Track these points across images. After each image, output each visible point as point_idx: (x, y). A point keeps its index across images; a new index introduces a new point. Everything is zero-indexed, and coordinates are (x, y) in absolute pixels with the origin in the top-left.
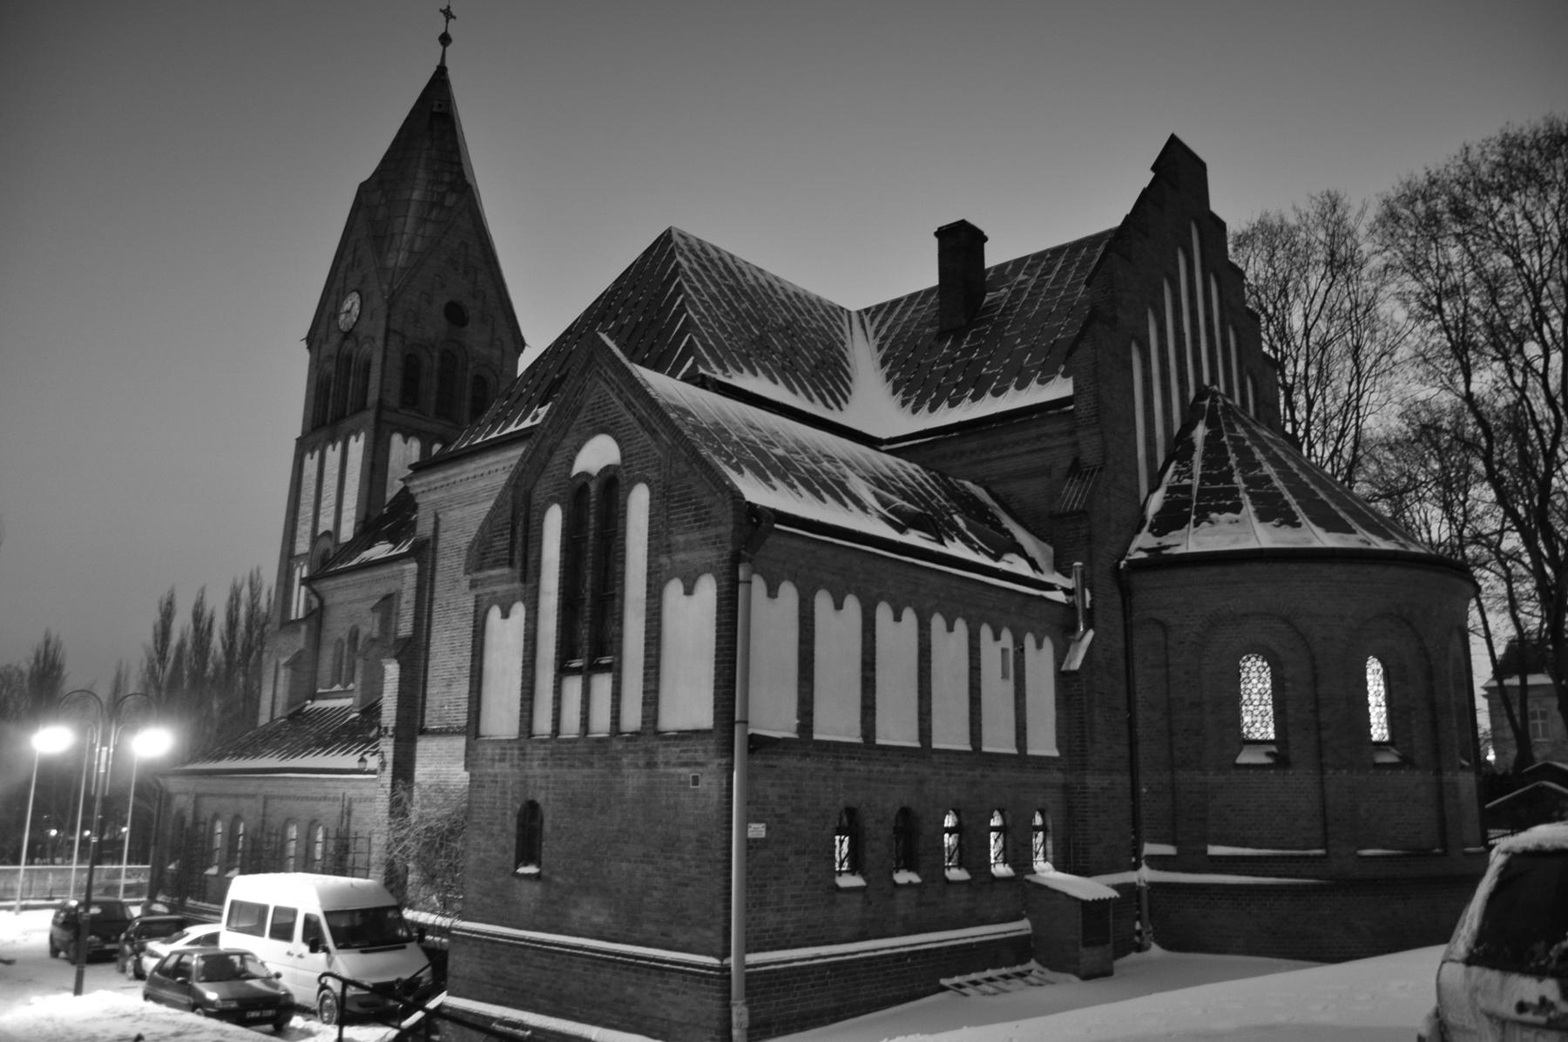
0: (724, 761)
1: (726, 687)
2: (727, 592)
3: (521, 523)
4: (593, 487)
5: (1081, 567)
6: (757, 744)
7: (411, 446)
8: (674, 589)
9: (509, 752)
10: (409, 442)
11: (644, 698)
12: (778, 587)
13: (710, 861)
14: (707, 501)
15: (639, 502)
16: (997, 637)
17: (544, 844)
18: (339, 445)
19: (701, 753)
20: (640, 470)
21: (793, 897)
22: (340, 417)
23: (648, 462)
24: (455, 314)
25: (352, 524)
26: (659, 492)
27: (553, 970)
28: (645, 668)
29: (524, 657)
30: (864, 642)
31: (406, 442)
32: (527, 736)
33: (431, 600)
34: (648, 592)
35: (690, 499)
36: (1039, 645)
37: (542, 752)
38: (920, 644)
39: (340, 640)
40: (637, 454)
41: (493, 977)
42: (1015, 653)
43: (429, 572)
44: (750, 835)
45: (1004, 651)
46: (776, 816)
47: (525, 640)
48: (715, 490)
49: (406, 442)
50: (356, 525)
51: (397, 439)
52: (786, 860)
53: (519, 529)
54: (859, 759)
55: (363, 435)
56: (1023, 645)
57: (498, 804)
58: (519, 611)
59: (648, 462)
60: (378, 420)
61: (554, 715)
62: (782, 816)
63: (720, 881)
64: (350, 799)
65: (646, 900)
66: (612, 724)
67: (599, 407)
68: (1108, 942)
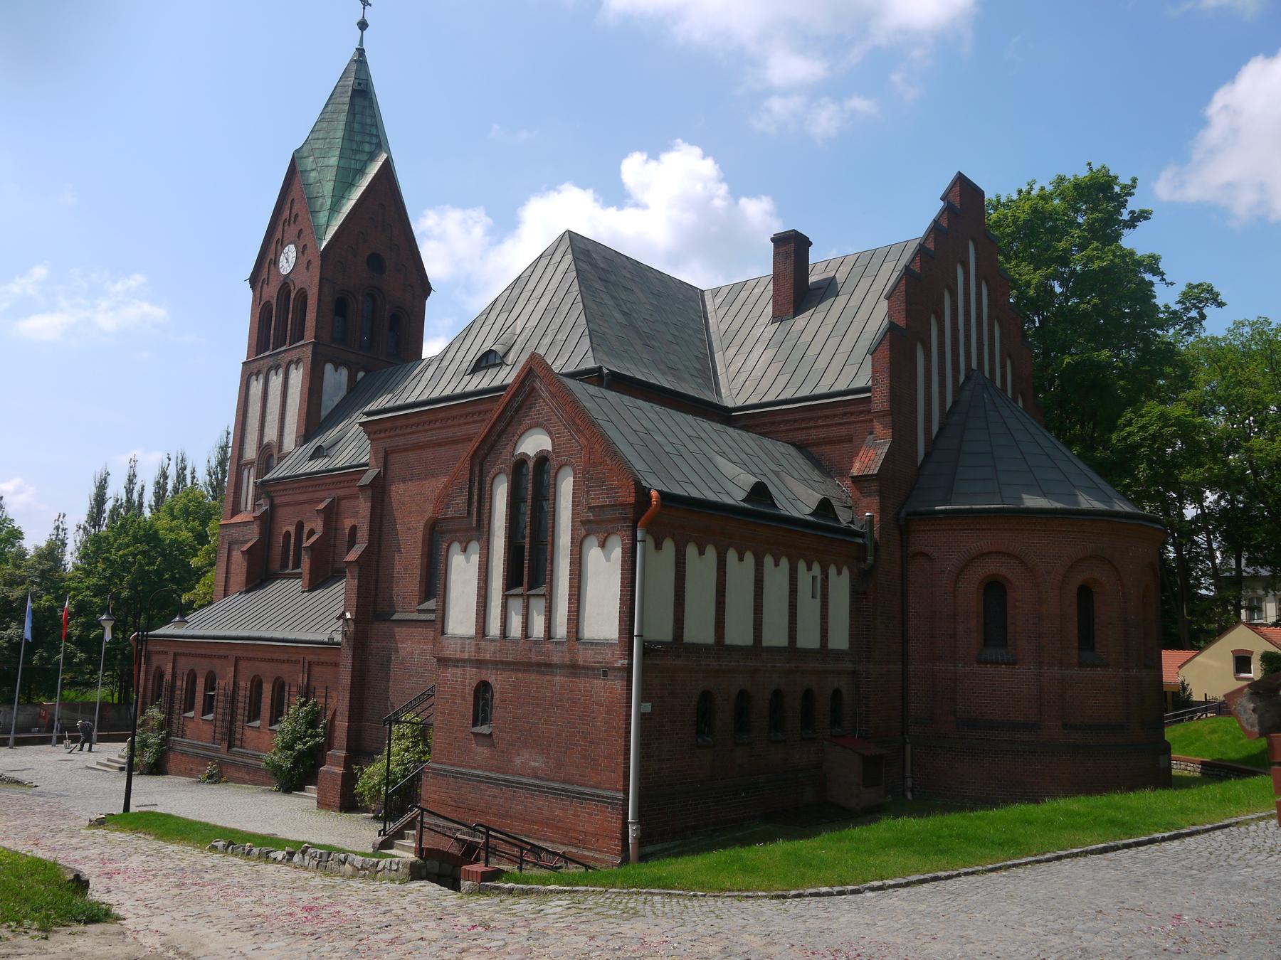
4: (531, 464)
7: (341, 374)
12: (662, 542)
16: (809, 569)
23: (572, 451)
24: (375, 262)
31: (336, 371)
36: (839, 573)
38: (756, 576)
39: (288, 534)
42: (822, 579)
45: (814, 578)
49: (336, 371)
51: (329, 368)
54: (713, 657)
55: (301, 364)
59: (572, 451)
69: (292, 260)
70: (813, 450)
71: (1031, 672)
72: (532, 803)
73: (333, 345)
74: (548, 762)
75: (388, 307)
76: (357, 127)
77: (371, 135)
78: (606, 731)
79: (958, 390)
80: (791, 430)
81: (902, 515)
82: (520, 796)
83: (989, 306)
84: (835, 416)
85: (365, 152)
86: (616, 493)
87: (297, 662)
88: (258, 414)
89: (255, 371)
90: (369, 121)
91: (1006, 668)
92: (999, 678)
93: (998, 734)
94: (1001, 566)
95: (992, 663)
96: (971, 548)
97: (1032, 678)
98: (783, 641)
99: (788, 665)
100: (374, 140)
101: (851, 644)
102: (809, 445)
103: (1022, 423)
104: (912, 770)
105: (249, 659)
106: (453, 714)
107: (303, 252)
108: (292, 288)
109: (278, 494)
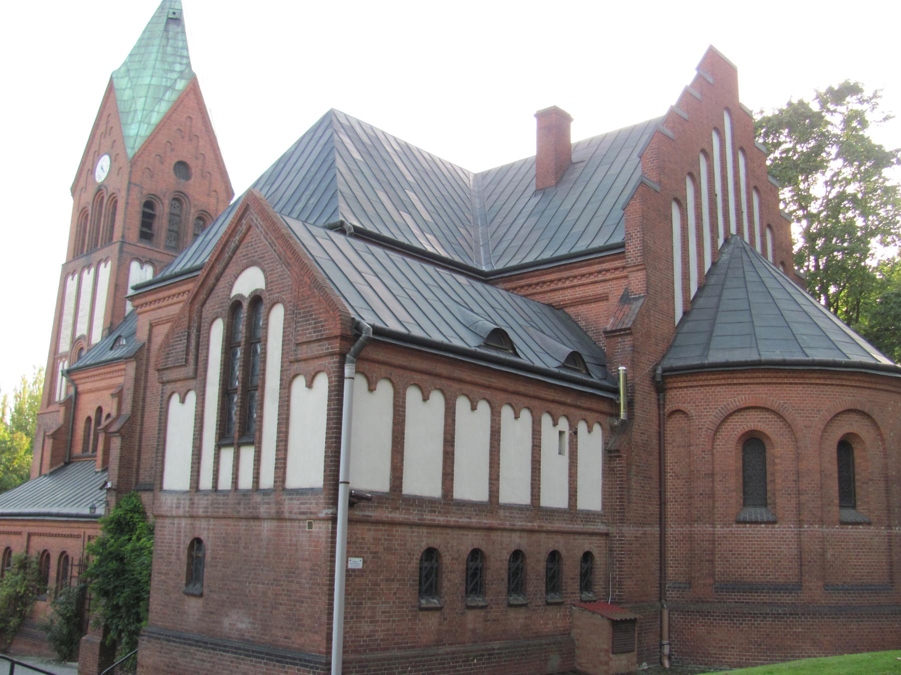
0: (330, 511)
1: (332, 457)
2: (335, 386)
3: (195, 331)
4: (245, 305)
5: (625, 370)
6: (355, 499)
7: (146, 271)
8: (299, 384)
9: (182, 502)
10: (144, 268)
11: (276, 464)
13: (319, 584)
14: (322, 317)
15: (276, 319)
16: (555, 424)
17: (205, 570)
18: (93, 270)
19: (314, 505)
20: (278, 293)
21: (383, 612)
22: (94, 247)
23: (283, 287)
24: (182, 168)
25: (101, 330)
26: (290, 310)
27: (209, 662)
28: (277, 441)
29: (194, 431)
30: (446, 425)
31: (142, 268)
32: (195, 490)
33: (145, 388)
34: (281, 385)
35: (311, 315)
37: (205, 502)
40: (276, 281)
41: (168, 666)
42: (570, 435)
43: (144, 367)
44: (350, 566)
45: (561, 433)
46: (371, 553)
47: (195, 419)
48: (329, 309)
49: (142, 268)
50: (103, 331)
52: (379, 585)
53: (193, 336)
55: (110, 263)
56: (576, 429)
57: (174, 540)
58: (192, 397)
60: (121, 251)
61: (214, 475)
62: (376, 553)
63: (325, 599)
64: (89, 536)
65: (274, 612)
66: (253, 482)
67: (252, 246)
68: (633, 651)
69: (107, 169)
70: (569, 310)
71: (792, 531)
72: (237, 667)
73: (139, 244)
74: (254, 624)
75: (193, 210)
76: (169, 50)
77: (182, 57)
78: (310, 588)
79: (716, 253)
80: (548, 292)
81: (659, 371)
82: (226, 661)
83: (747, 176)
84: (591, 274)
85: (175, 71)
86: (322, 326)
87: (78, 536)
88: (72, 311)
89: (72, 271)
90: (180, 44)
91: (766, 527)
92: (758, 538)
93: (758, 596)
94: (760, 422)
95: (751, 522)
96: (728, 404)
97: (792, 538)
98: (524, 498)
99: (529, 524)
100: (185, 61)
101: (604, 505)
102: (566, 306)
103: (801, 348)
104: (670, 637)
105: (41, 535)
106: (169, 574)
107: (115, 160)
108: (105, 194)
109: (82, 381)
